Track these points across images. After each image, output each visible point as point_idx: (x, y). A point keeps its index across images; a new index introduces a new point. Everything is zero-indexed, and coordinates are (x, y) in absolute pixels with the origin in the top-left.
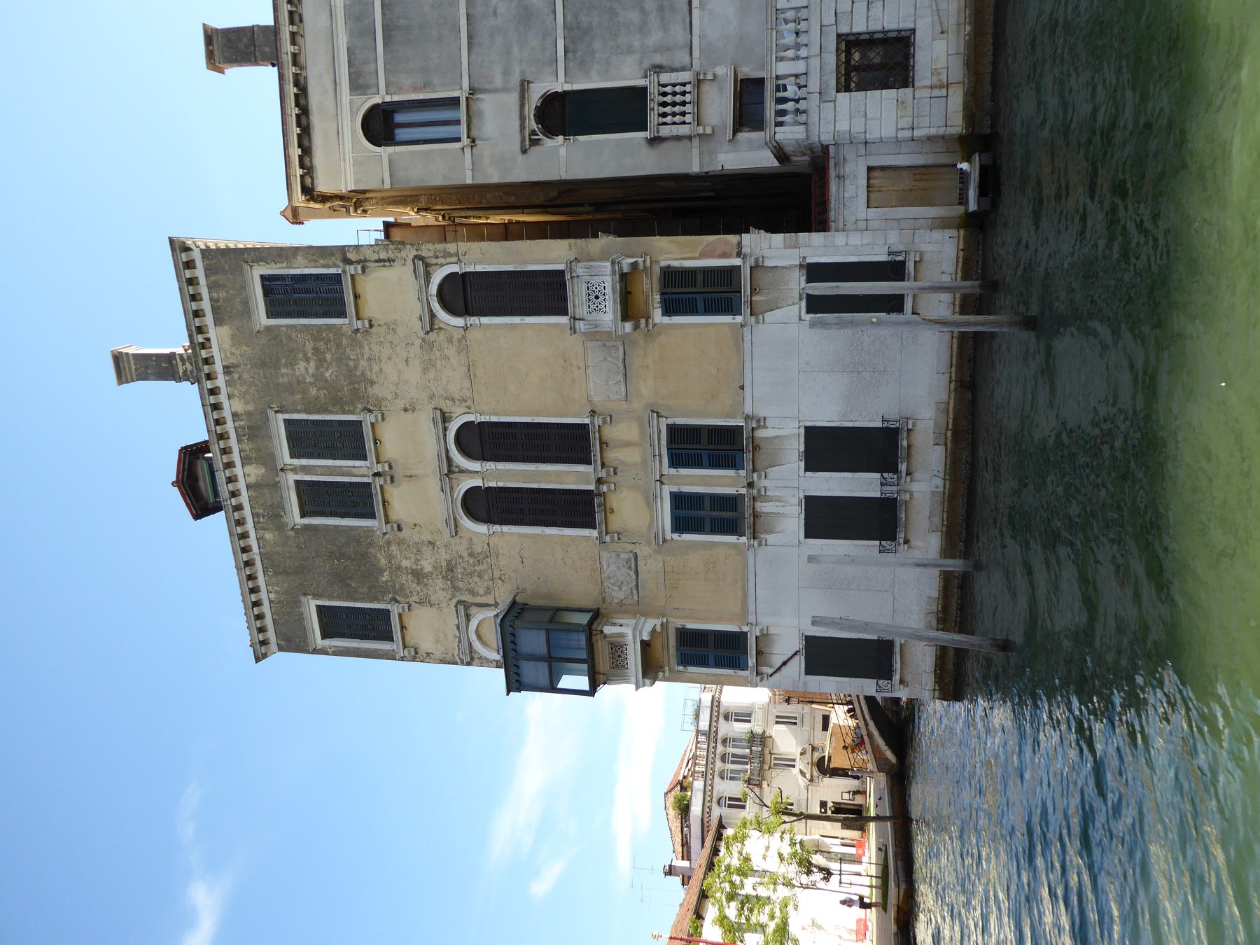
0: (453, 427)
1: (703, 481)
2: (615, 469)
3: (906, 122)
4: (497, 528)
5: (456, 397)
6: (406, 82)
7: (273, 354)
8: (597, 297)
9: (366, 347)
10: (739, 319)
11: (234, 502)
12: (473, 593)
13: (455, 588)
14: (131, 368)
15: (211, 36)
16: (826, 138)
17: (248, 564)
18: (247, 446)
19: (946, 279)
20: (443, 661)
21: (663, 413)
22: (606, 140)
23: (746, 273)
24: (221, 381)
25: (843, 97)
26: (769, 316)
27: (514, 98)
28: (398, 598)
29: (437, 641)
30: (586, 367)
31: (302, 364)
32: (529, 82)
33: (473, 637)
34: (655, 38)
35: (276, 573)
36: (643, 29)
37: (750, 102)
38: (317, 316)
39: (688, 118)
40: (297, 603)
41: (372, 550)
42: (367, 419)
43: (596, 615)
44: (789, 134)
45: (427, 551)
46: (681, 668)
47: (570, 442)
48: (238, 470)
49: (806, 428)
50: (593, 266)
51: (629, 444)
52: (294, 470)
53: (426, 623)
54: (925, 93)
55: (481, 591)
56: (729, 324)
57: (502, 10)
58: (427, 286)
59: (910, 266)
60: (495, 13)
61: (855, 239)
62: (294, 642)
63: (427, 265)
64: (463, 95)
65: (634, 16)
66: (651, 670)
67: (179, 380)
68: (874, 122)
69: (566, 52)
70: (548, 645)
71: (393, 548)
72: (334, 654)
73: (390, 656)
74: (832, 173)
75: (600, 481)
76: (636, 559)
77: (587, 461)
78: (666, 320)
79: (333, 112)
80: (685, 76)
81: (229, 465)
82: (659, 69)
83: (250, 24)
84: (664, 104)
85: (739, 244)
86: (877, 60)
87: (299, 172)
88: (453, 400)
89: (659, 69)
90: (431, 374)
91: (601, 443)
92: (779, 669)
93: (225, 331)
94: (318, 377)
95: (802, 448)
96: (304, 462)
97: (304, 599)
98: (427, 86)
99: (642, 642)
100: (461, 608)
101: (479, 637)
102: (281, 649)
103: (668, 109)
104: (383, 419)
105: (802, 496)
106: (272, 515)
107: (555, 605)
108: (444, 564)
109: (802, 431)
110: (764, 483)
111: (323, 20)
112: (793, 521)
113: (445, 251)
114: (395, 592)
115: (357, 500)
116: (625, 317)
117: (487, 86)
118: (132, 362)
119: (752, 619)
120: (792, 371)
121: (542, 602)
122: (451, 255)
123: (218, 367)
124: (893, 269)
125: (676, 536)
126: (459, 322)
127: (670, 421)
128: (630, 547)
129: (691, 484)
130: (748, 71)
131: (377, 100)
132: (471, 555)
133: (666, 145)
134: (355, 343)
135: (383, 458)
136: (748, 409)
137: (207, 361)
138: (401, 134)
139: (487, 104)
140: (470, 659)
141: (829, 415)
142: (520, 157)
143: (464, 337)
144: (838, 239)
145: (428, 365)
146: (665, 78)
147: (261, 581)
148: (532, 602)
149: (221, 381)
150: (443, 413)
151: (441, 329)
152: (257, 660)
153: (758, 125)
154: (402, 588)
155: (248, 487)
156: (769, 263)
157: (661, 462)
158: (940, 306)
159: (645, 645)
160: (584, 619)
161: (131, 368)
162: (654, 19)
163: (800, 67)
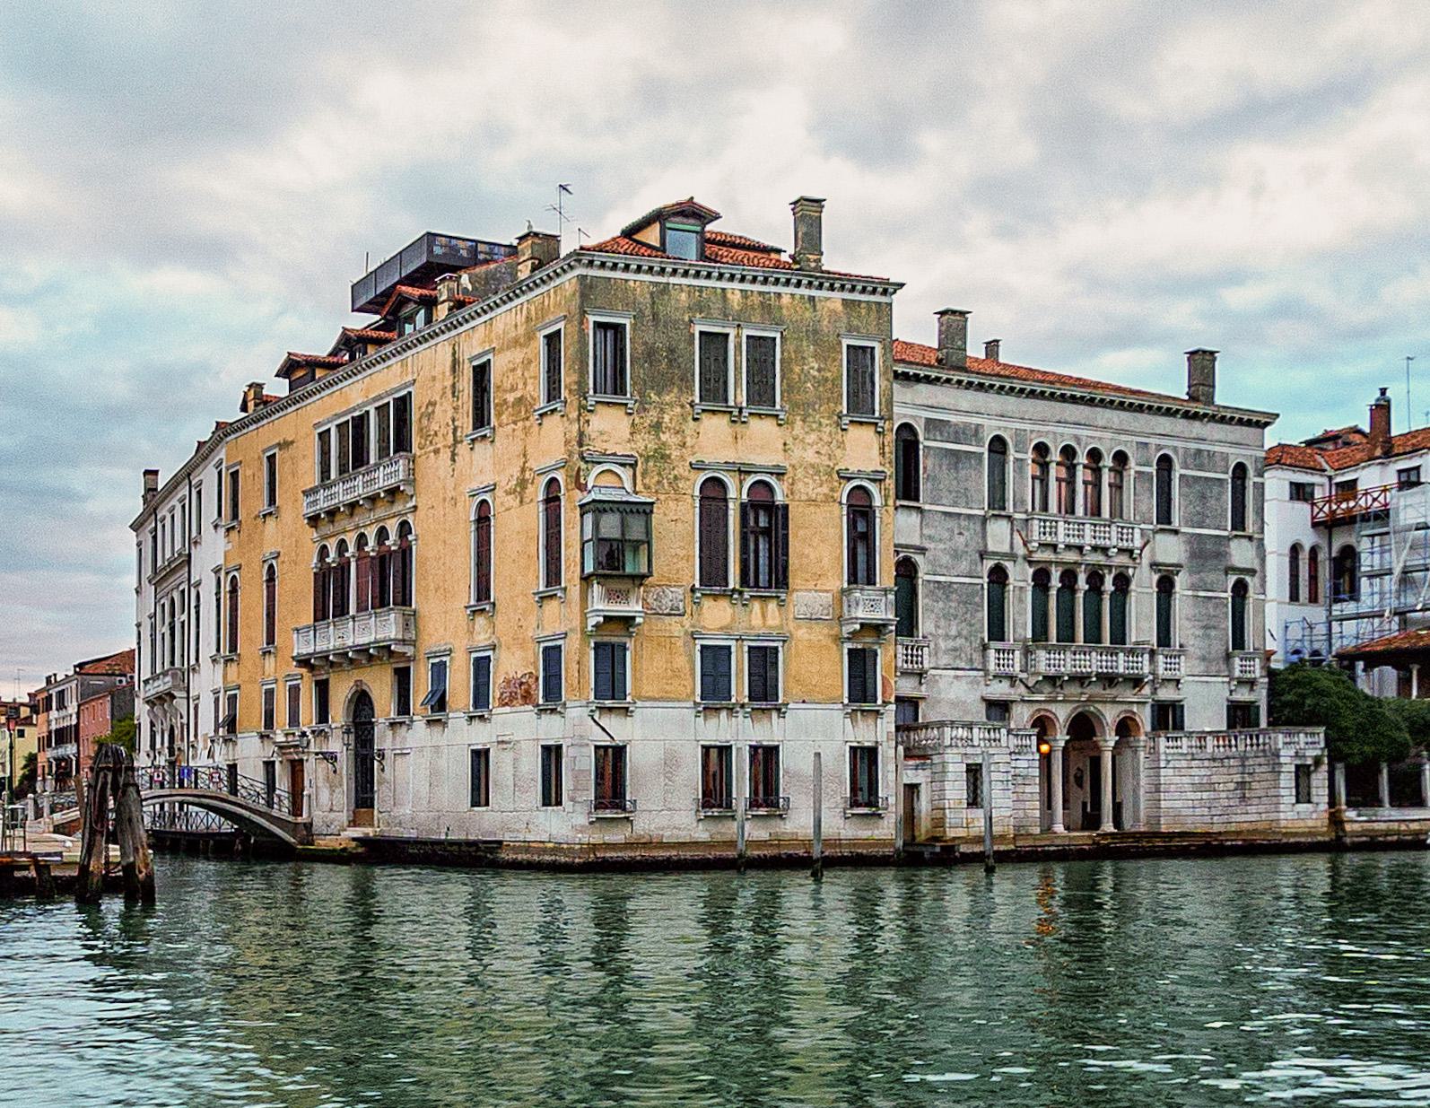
0: (772, 480)
6: (930, 463)
10: (846, 701)
27: (917, 542)
33: (606, 467)
36: (947, 636)
51: (764, 616)
55: (647, 481)
60: (960, 534)
65: (953, 632)
78: (846, 651)
99: (634, 618)
104: (780, 425)
111: (965, 406)
114: (641, 403)
115: (714, 390)
120: (814, 735)
123: (814, 292)
125: (698, 647)
128: (689, 611)
130: (922, 705)
131: (921, 438)
132: (676, 477)
139: (915, 518)
147: (648, 278)
150: (783, 474)
154: (645, 410)
155: (723, 289)
162: (951, 644)
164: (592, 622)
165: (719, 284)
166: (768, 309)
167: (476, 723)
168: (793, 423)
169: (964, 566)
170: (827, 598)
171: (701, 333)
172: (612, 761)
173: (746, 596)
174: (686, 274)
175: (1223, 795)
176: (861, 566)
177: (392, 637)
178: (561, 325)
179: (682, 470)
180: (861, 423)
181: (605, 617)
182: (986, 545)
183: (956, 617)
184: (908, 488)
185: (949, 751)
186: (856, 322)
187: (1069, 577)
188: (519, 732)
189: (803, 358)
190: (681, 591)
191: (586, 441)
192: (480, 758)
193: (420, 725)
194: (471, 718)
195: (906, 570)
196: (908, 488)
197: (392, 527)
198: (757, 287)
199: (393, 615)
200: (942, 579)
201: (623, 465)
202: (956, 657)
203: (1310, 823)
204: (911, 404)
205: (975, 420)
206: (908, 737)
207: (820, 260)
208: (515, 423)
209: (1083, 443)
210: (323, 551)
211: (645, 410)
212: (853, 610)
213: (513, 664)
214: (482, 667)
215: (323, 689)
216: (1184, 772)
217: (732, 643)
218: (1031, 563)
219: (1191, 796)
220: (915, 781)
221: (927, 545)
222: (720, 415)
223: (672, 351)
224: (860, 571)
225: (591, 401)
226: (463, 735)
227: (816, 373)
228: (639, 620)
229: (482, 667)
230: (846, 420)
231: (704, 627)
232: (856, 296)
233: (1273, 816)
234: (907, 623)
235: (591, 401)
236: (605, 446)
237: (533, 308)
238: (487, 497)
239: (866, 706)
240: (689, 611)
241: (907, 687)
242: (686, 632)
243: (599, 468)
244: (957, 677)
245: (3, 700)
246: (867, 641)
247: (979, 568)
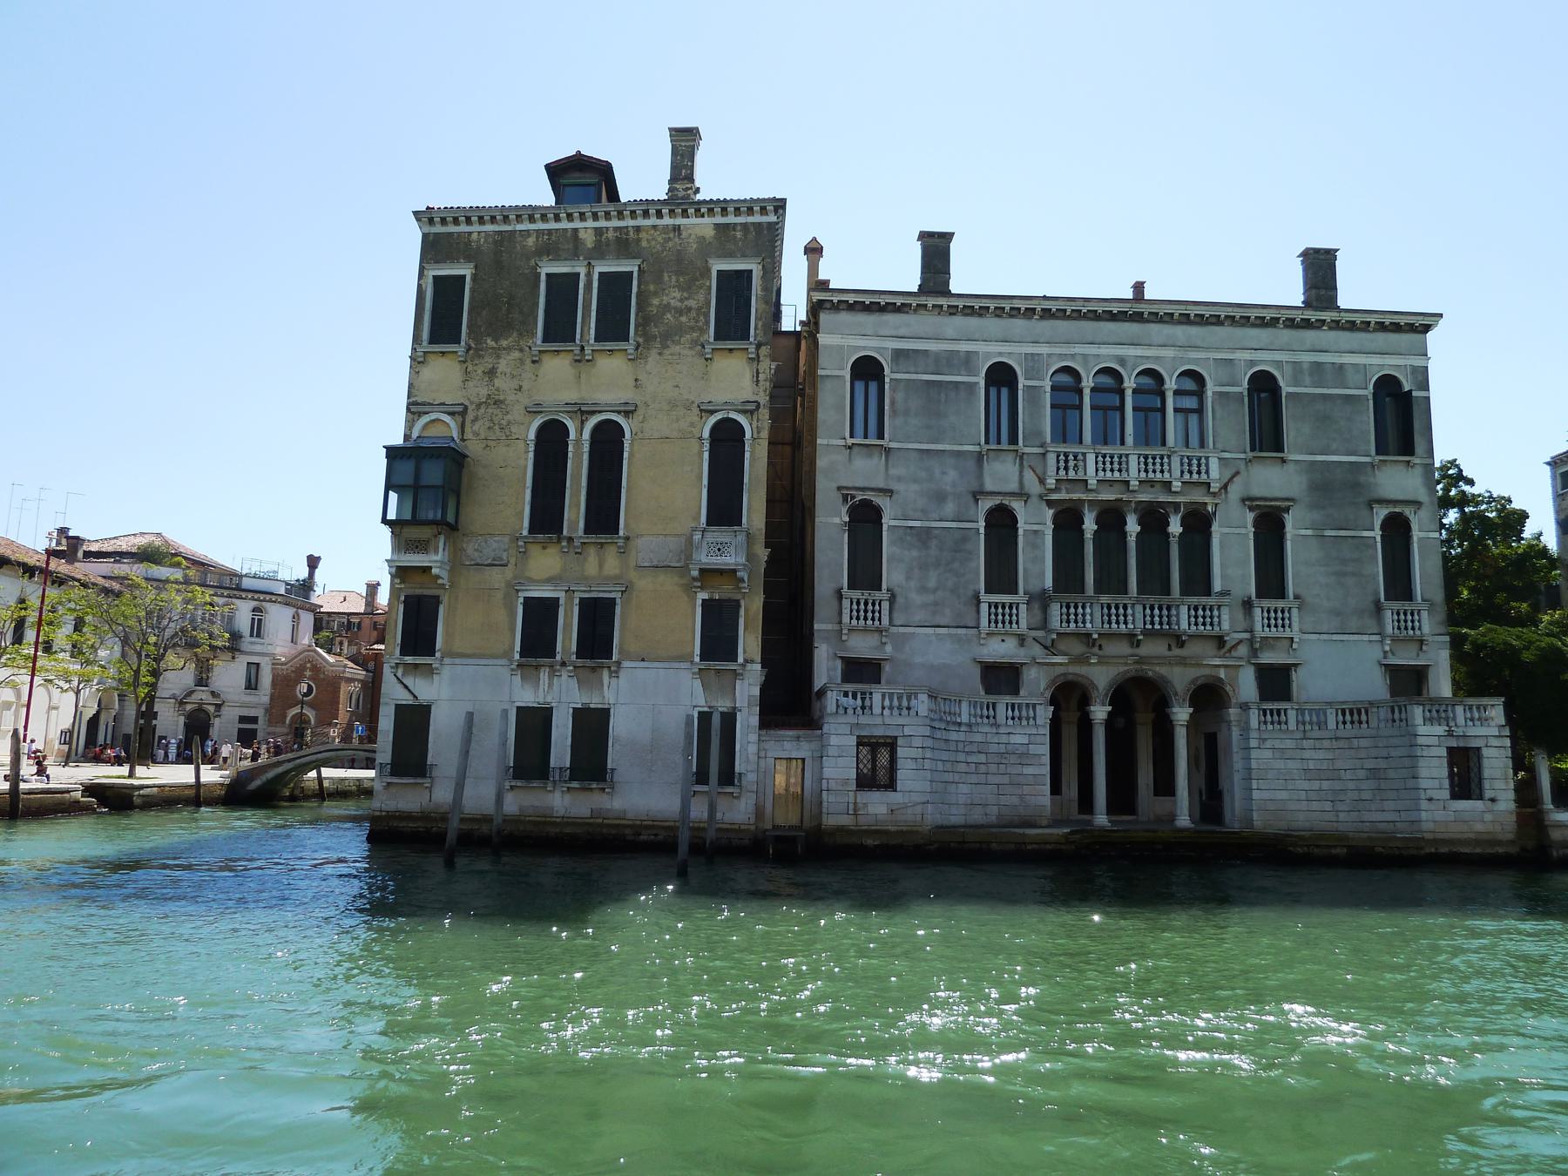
1: (567, 626)
3: (833, 785)
4: (532, 448)
7: (689, 270)
10: (697, 659)
11: (563, 215)
13: (479, 406)
14: (685, 142)
15: (947, 237)
16: (826, 727)
17: (506, 219)
18: (611, 234)
19: (719, 816)
20: (411, 386)
23: (732, 666)
25: (853, 741)
26: (698, 683)
27: (880, 483)
31: (677, 295)
33: (433, 416)
34: (917, 598)
35: (495, 242)
36: (923, 589)
37: (862, 671)
39: (854, 622)
40: (468, 259)
42: (630, 347)
43: (453, 528)
44: (831, 699)
45: (515, 384)
47: (603, 517)
48: (590, 224)
50: (739, 551)
51: (601, 566)
52: (589, 275)
53: (446, 373)
54: (852, 800)
58: (739, 411)
59: (730, 789)
61: (752, 749)
62: (433, 249)
63: (752, 412)
65: (932, 584)
66: (401, 573)
67: (671, 182)
68: (841, 766)
70: (427, 481)
71: (517, 354)
72: (419, 286)
73: (417, 338)
74: (801, 733)
75: (570, 539)
77: (587, 531)
78: (699, 602)
80: (885, 621)
81: (595, 217)
82: (892, 599)
84: (866, 604)
85: (752, 661)
86: (877, 769)
87: (835, 300)
89: (892, 599)
91: (602, 544)
93: (710, 233)
94: (667, 308)
96: (595, 284)
97: (472, 265)
98: (894, 412)
100: (460, 409)
102: (425, 236)
103: (862, 606)
106: (551, 246)
107: (463, 492)
110: (565, 677)
111: (950, 333)
112: (528, 697)
114: (477, 350)
115: (560, 329)
116: (701, 570)
119: (447, 660)
121: (465, 479)
123: (680, 221)
124: (728, 776)
128: (513, 561)
130: (887, 668)
132: (509, 423)
133: (835, 603)
134: (694, 343)
135: (597, 355)
136: (625, 664)
137: (685, 214)
138: (860, 386)
140: (415, 408)
141: (618, 726)
142: (835, 485)
144: (753, 737)
145: (673, 405)
146: (885, 605)
147: (489, 228)
148: (465, 471)
149: (667, 221)
152: (415, 213)
153: (846, 678)
154: (480, 356)
155: (576, 230)
158: (699, 811)
159: (426, 570)
160: (450, 518)
161: (685, 142)
163: (877, 710)
169: (950, 508)
175: (1351, 785)
179: (517, 413)
182: (982, 485)
187: (1111, 518)
200: (911, 523)
203: (1479, 827)
205: (964, 347)
209: (1129, 364)
216: (1289, 754)
218: (1050, 503)
219: (1306, 785)
221: (893, 486)
233: (1413, 816)
240: (513, 561)
247: (972, 512)
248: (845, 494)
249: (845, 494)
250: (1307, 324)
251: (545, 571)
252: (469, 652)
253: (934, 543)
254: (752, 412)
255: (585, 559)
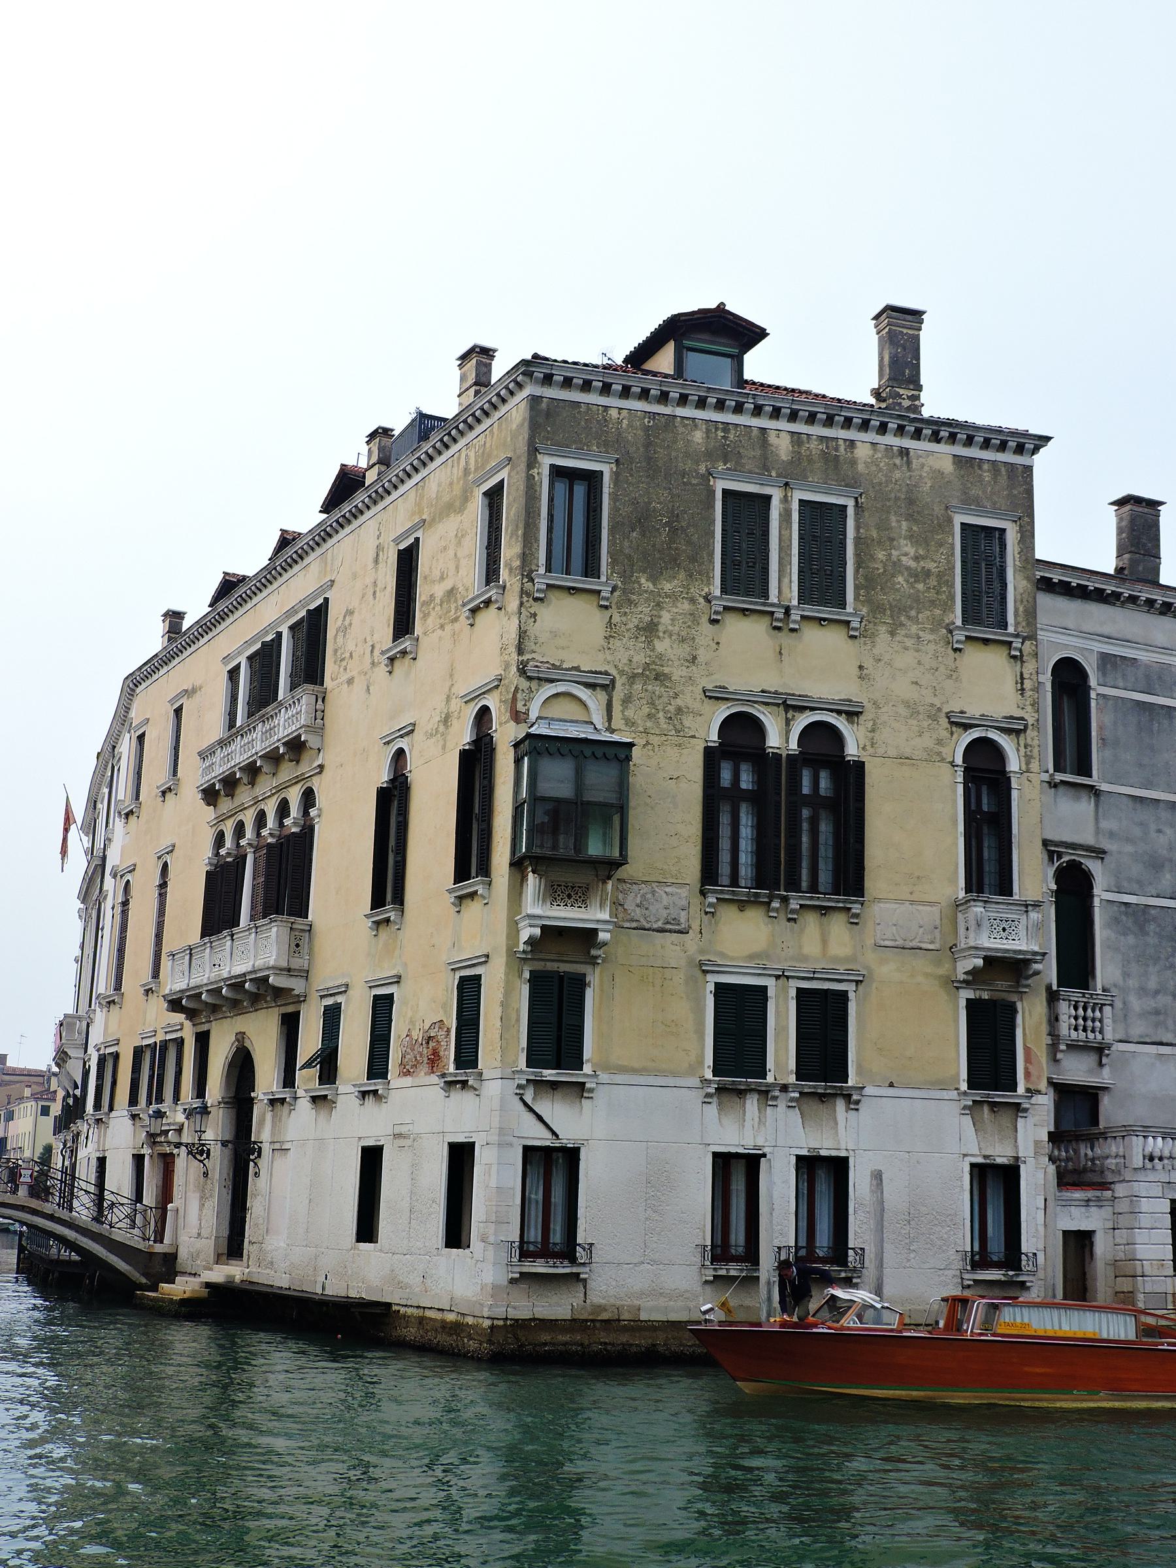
0: (840, 723)
1: (782, 1030)
2: (795, 920)
5: (877, 735)
6: (1108, 719)
8: (1004, 930)
9: (931, 637)
10: (964, 1086)
12: (627, 701)
13: (633, 678)
21: (861, 987)
22: (1050, 939)
24: (890, 439)
26: (967, 1121)
27: (1088, 839)
28: (617, 594)
29: (555, 634)
30: (912, 902)
31: (912, 551)
32: (1102, 859)
33: (561, 688)
34: (1136, 1004)
36: (1143, 991)
38: (963, 584)
41: (682, 575)
45: (683, 651)
46: (527, 975)
49: (847, 1158)
51: (825, 942)
55: (629, 713)
56: (958, 1074)
57: (1163, 840)
60: (1159, 831)
63: (1018, 732)
64: (1095, 780)
65: (1152, 984)
69: (1126, 904)
71: (686, 606)
76: (682, 932)
78: (963, 1003)
79: (1084, 629)
83: (1162, 556)
85: (1039, 1092)
88: (873, 731)
90: (903, 711)
92: (531, 1110)
95: (823, 1153)
96: (795, 516)
99: (594, 932)
101: (557, 695)
104: (852, 637)
105: (766, 1150)
108: (666, 670)
109: (843, 1154)
113: (1032, 757)
114: (624, 591)
115: (745, 576)
117: (1100, 810)
118: (911, 332)
120: (909, 1146)
122: (1028, 763)
123: (907, 443)
125: (711, 987)
126: (959, 760)
127: (851, 995)
128: (695, 925)
129: (777, 1012)
130: (1105, 1102)
131: (1093, 682)
132: (679, 710)
134: (937, 624)
139: (1085, 806)
143: (943, 760)
145: (913, 709)
150: (858, 714)
151: (952, 734)
154: (630, 602)
155: (763, 430)
156: (1021, 1123)
157: (803, 978)
162: (1151, 1003)
164: (524, 936)
165: (756, 422)
166: (834, 464)
167: (370, 1100)
168: (873, 636)
170: (930, 915)
171: (726, 492)
172: (553, 1168)
173: (794, 905)
174: (701, 403)
176: (990, 867)
177: (272, 963)
178: (503, 474)
179: (691, 698)
180: (986, 641)
181: (543, 928)
183: (1156, 960)
184: (1073, 752)
185: (1141, 1176)
186: (974, 492)
188: (420, 1117)
189: (892, 540)
190: (684, 892)
191: (529, 645)
192: (372, 1159)
193: (304, 1104)
194: (364, 1094)
195: (1073, 887)
196: (1073, 752)
197: (294, 796)
198: (817, 430)
199: (275, 929)
201: (592, 686)
202: (1157, 1025)
204: (1068, 630)
206: (1076, 1151)
207: (918, 398)
208: (442, 627)
210: (220, 839)
211: (630, 602)
212: (972, 934)
213: (425, 1007)
214: (382, 1007)
215: (203, 1040)
217: (770, 983)
220: (1084, 1226)
221: (1105, 844)
222: (754, 617)
223: (674, 517)
224: (988, 871)
225: (540, 583)
226: (356, 1122)
227: (912, 564)
228: (603, 936)
229: (382, 1007)
230: (960, 636)
231: (722, 955)
232: (974, 452)
234: (1077, 964)
235: (540, 583)
236: (562, 655)
237: (472, 454)
238: (402, 744)
239: (999, 1097)
240: (695, 925)
241: (1077, 1070)
242: (690, 961)
243: (549, 690)
244: (1160, 1055)
245: (11, 1063)
246: (1000, 988)
248: (1051, 848)
249: (1051, 848)
250: (1112, 599)
251: (749, 941)
252: (636, 1065)
253: (1152, 927)
254: (1018, 732)
255: (802, 930)
